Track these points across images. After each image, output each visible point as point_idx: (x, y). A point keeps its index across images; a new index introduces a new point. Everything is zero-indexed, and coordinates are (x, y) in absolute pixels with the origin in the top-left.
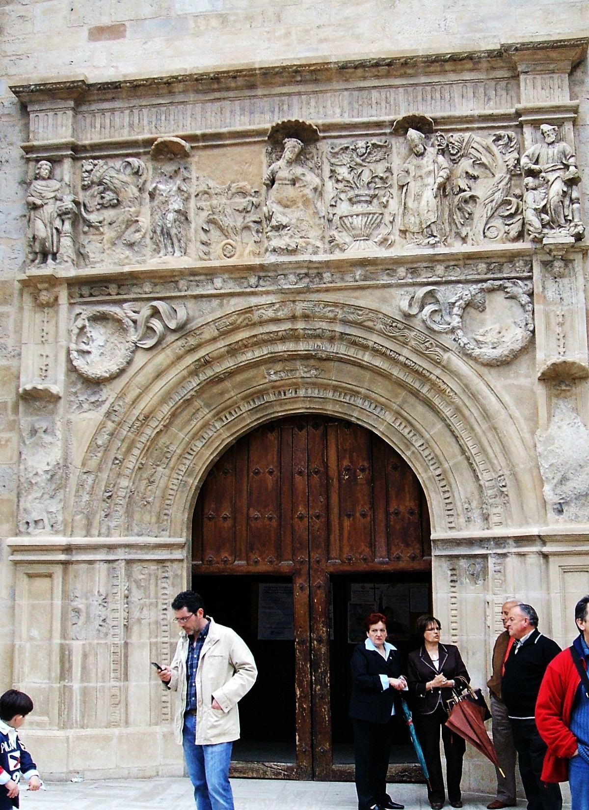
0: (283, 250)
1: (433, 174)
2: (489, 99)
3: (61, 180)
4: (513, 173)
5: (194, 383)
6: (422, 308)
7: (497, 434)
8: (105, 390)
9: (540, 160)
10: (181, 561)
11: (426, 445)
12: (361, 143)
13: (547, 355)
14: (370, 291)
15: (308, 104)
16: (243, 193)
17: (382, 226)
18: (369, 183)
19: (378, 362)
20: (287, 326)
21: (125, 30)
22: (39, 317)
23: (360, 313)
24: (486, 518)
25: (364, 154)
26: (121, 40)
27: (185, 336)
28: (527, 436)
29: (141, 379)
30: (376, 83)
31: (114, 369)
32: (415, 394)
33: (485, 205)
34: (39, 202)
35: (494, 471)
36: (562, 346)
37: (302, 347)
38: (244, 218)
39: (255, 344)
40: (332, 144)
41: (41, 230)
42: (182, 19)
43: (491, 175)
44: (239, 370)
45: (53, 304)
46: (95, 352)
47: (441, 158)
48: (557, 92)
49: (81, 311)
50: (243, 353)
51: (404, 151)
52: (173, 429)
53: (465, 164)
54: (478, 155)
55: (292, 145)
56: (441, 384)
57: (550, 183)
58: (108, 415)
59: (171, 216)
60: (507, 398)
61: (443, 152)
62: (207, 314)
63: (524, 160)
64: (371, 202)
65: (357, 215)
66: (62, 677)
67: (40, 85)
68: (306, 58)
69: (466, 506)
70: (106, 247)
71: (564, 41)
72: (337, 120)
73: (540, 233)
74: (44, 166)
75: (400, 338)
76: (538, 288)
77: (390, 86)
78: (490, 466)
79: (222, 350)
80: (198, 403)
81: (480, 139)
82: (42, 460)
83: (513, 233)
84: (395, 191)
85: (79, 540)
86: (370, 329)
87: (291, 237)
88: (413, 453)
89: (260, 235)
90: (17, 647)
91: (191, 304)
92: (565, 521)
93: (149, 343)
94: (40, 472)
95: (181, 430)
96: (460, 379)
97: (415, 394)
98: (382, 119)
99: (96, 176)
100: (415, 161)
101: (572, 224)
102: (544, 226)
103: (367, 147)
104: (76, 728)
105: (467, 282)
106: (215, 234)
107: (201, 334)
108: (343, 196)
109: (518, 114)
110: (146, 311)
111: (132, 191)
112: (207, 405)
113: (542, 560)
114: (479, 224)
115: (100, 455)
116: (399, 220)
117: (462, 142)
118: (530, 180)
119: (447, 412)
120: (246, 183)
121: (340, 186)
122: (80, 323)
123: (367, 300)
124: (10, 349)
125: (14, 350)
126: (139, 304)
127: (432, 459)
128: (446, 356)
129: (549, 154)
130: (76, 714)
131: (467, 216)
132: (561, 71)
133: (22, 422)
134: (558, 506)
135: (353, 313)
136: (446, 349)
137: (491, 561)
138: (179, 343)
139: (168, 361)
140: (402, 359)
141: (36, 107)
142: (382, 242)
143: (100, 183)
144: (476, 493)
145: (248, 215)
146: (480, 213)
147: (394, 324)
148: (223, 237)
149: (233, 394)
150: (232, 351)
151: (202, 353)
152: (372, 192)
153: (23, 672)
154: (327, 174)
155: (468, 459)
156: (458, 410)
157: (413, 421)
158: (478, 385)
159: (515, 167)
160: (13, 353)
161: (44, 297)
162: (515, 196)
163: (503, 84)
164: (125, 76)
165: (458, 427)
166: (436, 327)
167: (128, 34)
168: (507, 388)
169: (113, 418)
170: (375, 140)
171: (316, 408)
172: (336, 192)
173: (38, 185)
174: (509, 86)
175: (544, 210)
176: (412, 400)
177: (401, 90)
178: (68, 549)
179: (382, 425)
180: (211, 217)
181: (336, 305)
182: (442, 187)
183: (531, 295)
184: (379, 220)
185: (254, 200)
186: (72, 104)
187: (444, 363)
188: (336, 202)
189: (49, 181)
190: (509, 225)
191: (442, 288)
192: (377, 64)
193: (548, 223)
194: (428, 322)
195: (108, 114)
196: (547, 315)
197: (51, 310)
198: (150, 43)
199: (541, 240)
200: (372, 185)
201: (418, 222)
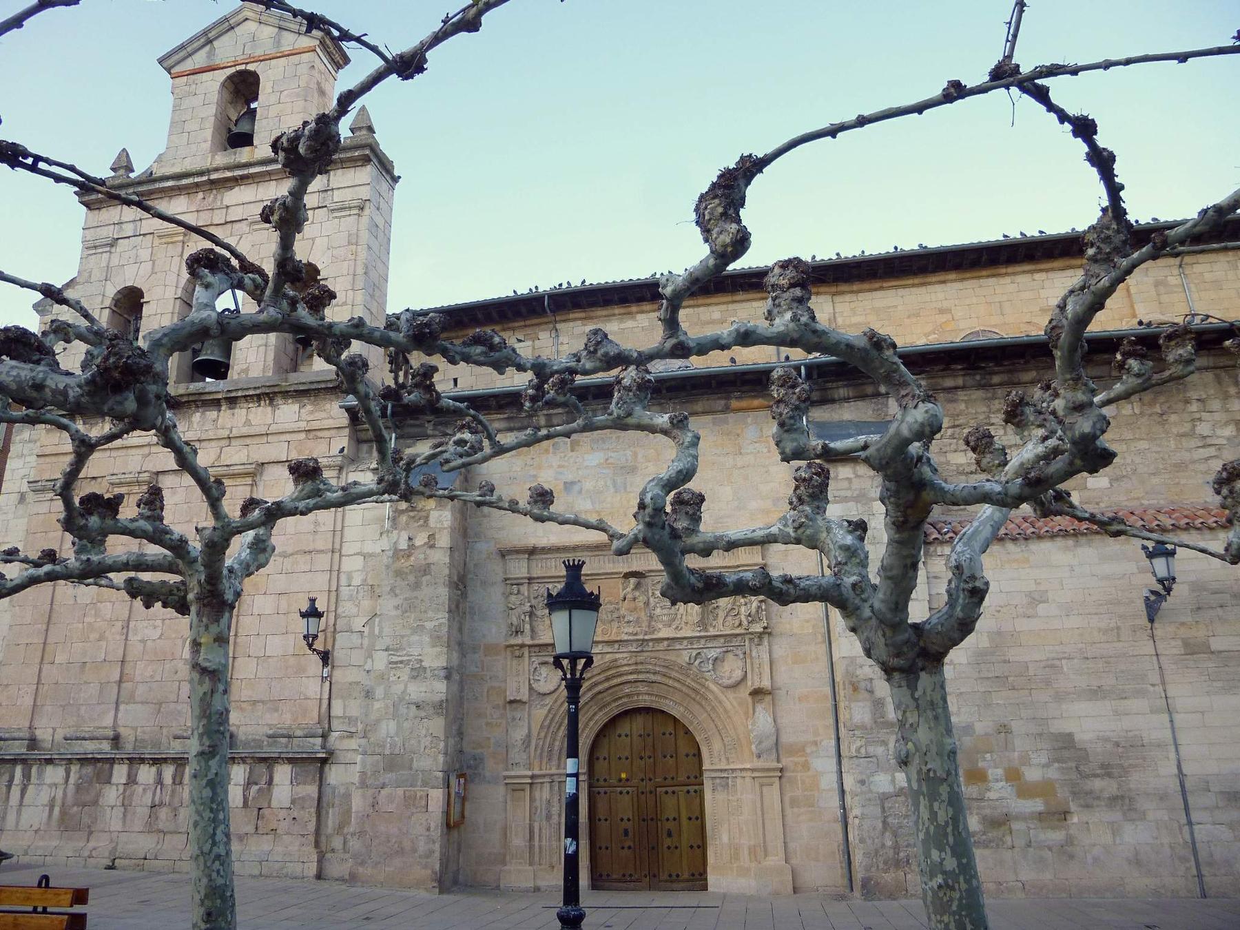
13: (751, 684)
19: (676, 685)
20: (633, 667)
22: (515, 662)
31: (552, 689)
37: (641, 677)
41: (515, 621)
46: (543, 680)
55: (633, 581)
58: (549, 711)
60: (735, 704)
82: (519, 734)
85: (537, 772)
130: (537, 859)
146: (721, 614)
150: (607, 679)
158: (722, 697)
161: (517, 653)
165: (713, 716)
168: (735, 698)
171: (648, 704)
173: (513, 598)
175: (750, 615)
178: (532, 777)
179: (676, 711)
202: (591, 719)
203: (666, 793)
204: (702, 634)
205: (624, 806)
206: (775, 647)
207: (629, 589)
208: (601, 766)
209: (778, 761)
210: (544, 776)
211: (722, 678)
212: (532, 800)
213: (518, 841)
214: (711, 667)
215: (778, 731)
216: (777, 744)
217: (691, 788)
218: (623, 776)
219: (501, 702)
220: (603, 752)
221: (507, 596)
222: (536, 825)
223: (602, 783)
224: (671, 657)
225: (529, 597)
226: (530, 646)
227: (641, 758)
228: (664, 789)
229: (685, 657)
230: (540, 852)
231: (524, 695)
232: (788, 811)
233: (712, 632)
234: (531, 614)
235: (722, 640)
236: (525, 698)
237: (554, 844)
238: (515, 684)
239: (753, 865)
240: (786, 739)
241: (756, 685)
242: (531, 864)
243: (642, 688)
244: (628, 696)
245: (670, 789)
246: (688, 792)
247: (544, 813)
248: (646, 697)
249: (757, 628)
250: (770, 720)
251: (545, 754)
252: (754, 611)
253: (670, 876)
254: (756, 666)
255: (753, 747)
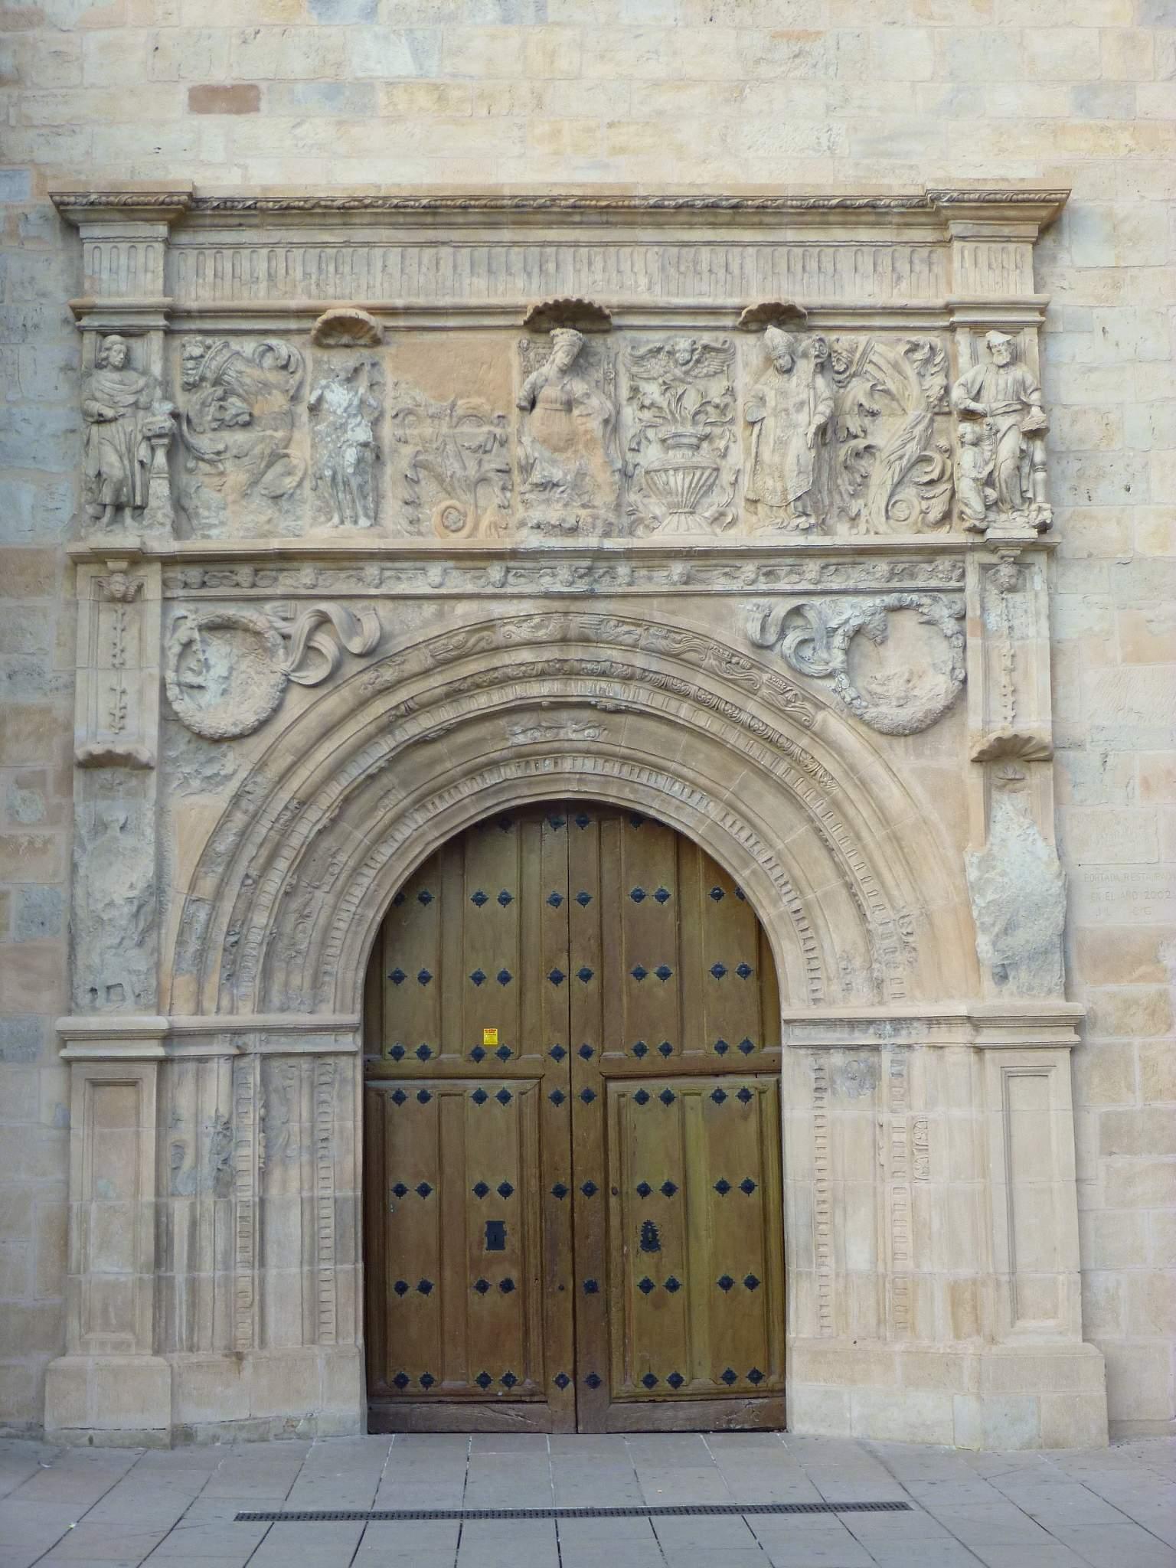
0: (554, 527)
1: (806, 409)
2: (899, 278)
3: (145, 372)
4: (936, 410)
5: (385, 746)
6: (782, 635)
7: (901, 848)
8: (231, 755)
10: (353, 1054)
11: (778, 859)
12: (683, 343)
14: (696, 600)
16: (475, 417)
17: (716, 490)
18: (697, 413)
19: (703, 720)
20: (553, 653)
21: (258, 98)
22: (107, 619)
23: (678, 637)
24: (878, 985)
25: (688, 362)
26: (252, 114)
27: (379, 664)
28: (951, 853)
29: (297, 738)
30: (709, 235)
31: (250, 720)
32: (765, 775)
33: (890, 464)
34: (109, 413)
35: (893, 908)
36: (1010, 707)
37: (579, 689)
38: (480, 462)
39: (492, 683)
40: (633, 340)
41: (114, 465)
42: (365, 86)
43: (900, 412)
44: (463, 724)
45: (130, 599)
46: (213, 688)
47: (820, 382)
49: (185, 613)
50: (472, 696)
51: (756, 359)
52: (345, 826)
53: (857, 391)
54: (879, 375)
55: (565, 338)
56: (808, 761)
57: (999, 435)
58: (236, 799)
59: (351, 455)
60: (919, 791)
61: (822, 367)
62: (416, 626)
63: (957, 394)
64: (698, 447)
66: (158, 1262)
67: (108, 194)
68: (593, 185)
69: (843, 965)
70: (230, 498)
71: (1030, 192)
72: (644, 298)
74: (117, 347)
75: (744, 683)
76: (974, 609)
78: (885, 901)
79: (438, 691)
80: (387, 780)
82: (119, 882)
83: (935, 514)
84: (739, 429)
85: (184, 1019)
86: (694, 666)
88: (754, 872)
89: (508, 494)
90: (75, 1210)
91: (384, 609)
92: (1012, 994)
93: (314, 675)
94: (119, 901)
95: (357, 827)
96: (842, 756)
97: (765, 775)
98: (720, 301)
99: (212, 366)
100: (775, 380)
101: (1034, 506)
102: (988, 508)
103: (693, 351)
104: (181, 1350)
105: (857, 592)
106: (428, 488)
107: (403, 663)
108: (651, 433)
109: (949, 309)
110: (304, 621)
111: (278, 401)
112: (404, 784)
113: (973, 1057)
115: (220, 870)
116: (745, 481)
117: (852, 351)
119: (818, 808)
120: (483, 400)
121: (647, 415)
122: (183, 635)
123: (692, 618)
124: (49, 676)
125: (57, 678)
126: (293, 603)
127: (786, 883)
128: (820, 716)
129: (997, 388)
131: (859, 480)
132: (1020, 239)
133: (80, 810)
134: (999, 970)
135: (666, 638)
136: (820, 706)
137: (886, 1057)
138: (366, 677)
139: (344, 709)
140: (744, 717)
141: (97, 231)
142: (716, 519)
143: (217, 382)
144: (860, 943)
145: (486, 457)
146: (881, 475)
147: (734, 660)
148: (443, 495)
149: (448, 765)
150: (454, 694)
151: (402, 695)
152: (702, 430)
153: (86, 1256)
154: (624, 393)
155: (849, 886)
156: (836, 804)
157: (757, 821)
158: (870, 765)
159: (941, 399)
160: (53, 684)
161: (118, 585)
162: (939, 449)
164: (265, 188)
165: (835, 833)
166: (807, 669)
167: (263, 105)
169: (244, 804)
170: (706, 338)
171: (591, 791)
172: (639, 426)
173: (107, 380)
175: (989, 481)
176: (758, 784)
178: (169, 1037)
179: (690, 815)
180: (421, 457)
181: (637, 622)
182: (822, 430)
183: (961, 618)
185: (498, 431)
186: (162, 230)
187: (816, 728)
188: (639, 444)
189: (124, 373)
191: (816, 601)
193: (996, 503)
194: (794, 661)
195: (228, 253)
196: (986, 654)
197: (129, 608)
198: (306, 126)
200: (702, 418)
201: (779, 489)
202: (382, 837)
203: (642, 1098)
204: (816, 540)
205: (491, 1144)
206: (1069, 601)
207: (549, 370)
208: (410, 1005)
209: (1068, 993)
210: (208, 1034)
211: (876, 698)
212: (165, 1120)
213: (112, 1265)
214: (838, 659)
215: (1069, 890)
216: (1064, 935)
217: (730, 1085)
218: (490, 1038)
219: (46, 760)
220: (415, 955)
221: (79, 374)
222: (180, 1212)
223: (411, 1061)
224: (692, 618)
225: (166, 384)
226: (169, 561)
227: (557, 978)
228: (634, 1087)
229: (745, 620)
230: (193, 1305)
231: (142, 736)
232: (1097, 1167)
233: (844, 535)
234: (176, 444)
235: (882, 567)
236: (147, 751)
237: (244, 1274)
238: (105, 704)
239: (970, 1347)
240: (1092, 919)
241: (1001, 728)
242: (159, 1349)
243: (574, 731)
244: (523, 756)
245: (655, 1088)
246: (719, 1097)
247: (207, 1170)
248: (588, 765)
249: (1016, 526)
250: (1045, 850)
251: (216, 957)
252: (1006, 468)
253: (650, 1381)
254: (999, 664)
255: (983, 943)
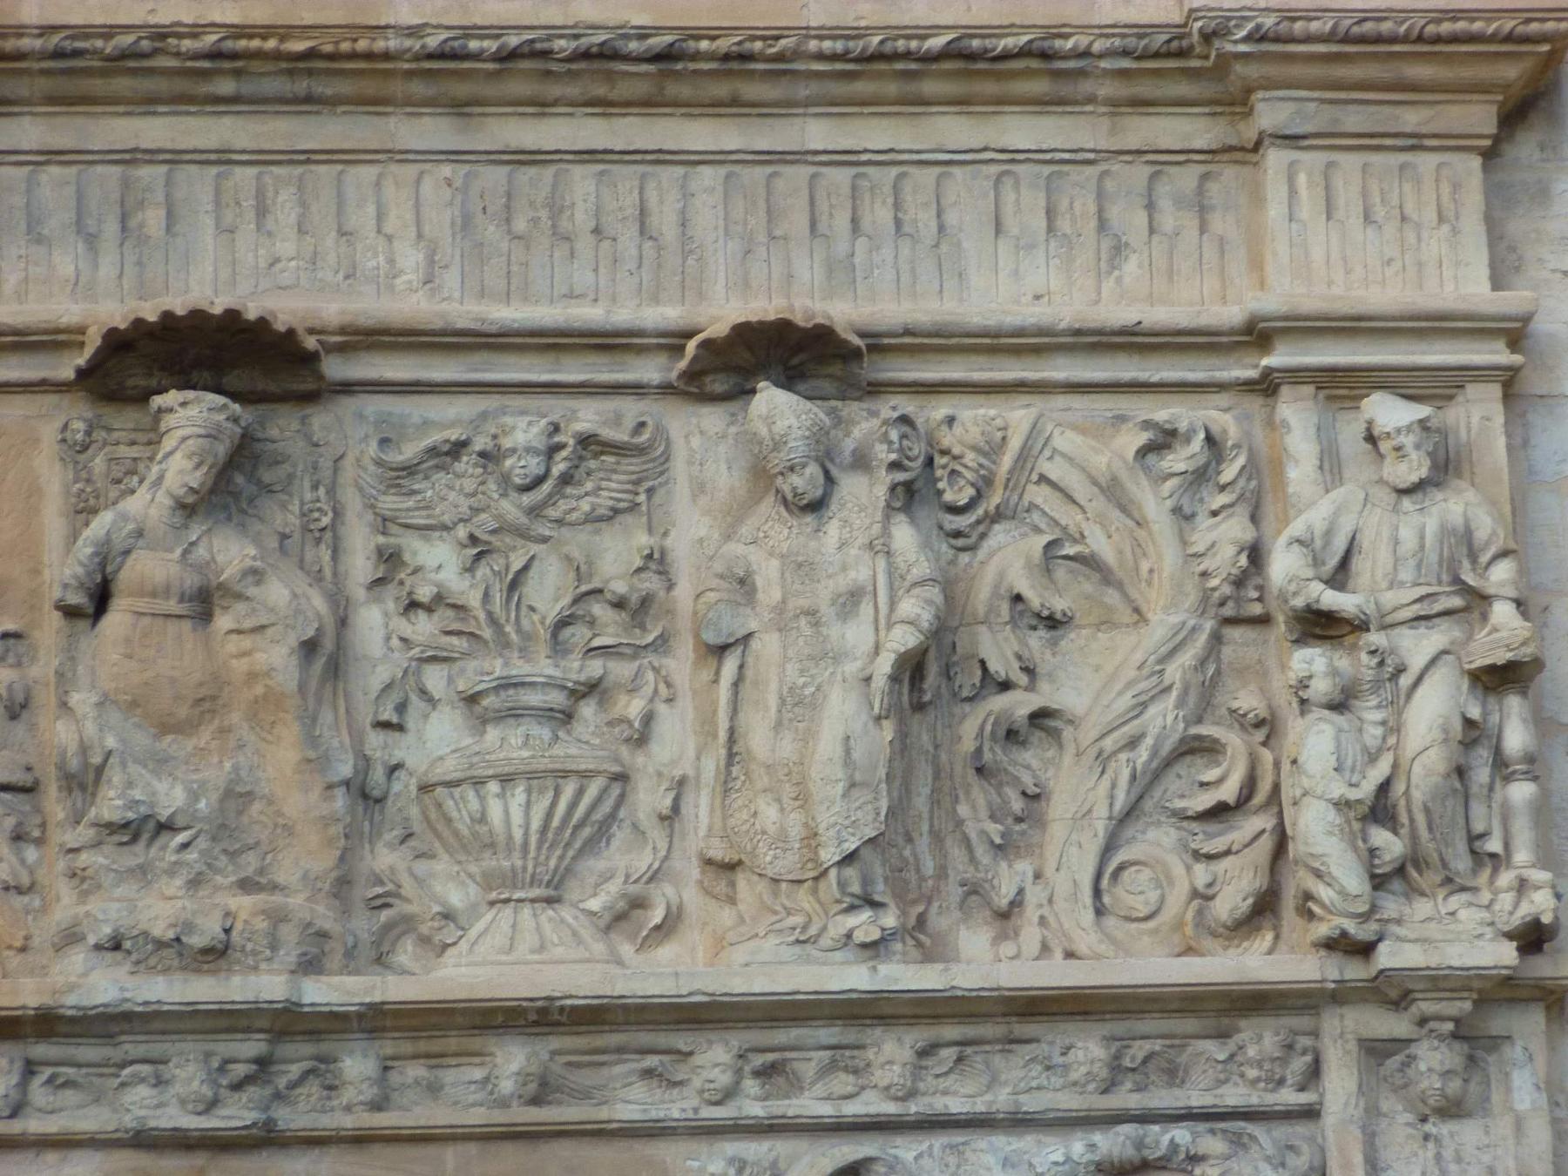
0: (160, 944)
1: (866, 609)
2: (1119, 249)
4: (1229, 611)
9: (1358, 564)
12: (523, 430)
15: (262, 211)
17: (620, 835)
18: (563, 623)
25: (539, 481)
33: (1104, 760)
40: (382, 420)
43: (1127, 617)
47: (904, 535)
48: (1434, 244)
51: (726, 477)
53: (1008, 558)
54: (1068, 517)
55: (191, 419)
57: (1405, 681)
63: (1284, 565)
64: (568, 717)
65: (506, 780)
72: (409, 305)
73: (1365, 917)
77: (661, 157)
81: (1081, 445)
83: (1232, 900)
84: (681, 664)
87: (195, 883)
89: (31, 854)
98: (624, 315)
100: (785, 532)
102: (1378, 882)
105: (1019, 1122)
108: (435, 678)
114: (1069, 849)
116: (701, 808)
118: (1314, 663)
121: (423, 627)
129: (1397, 549)
131: (1017, 805)
142: (620, 917)
146: (1079, 794)
152: (577, 669)
154: (360, 566)
159: (1239, 582)
162: (1239, 719)
163: (1186, 178)
170: (588, 416)
172: (401, 658)
174: (1213, 188)
175: (1380, 809)
177: (708, 176)
182: (912, 668)
184: (606, 807)
188: (401, 708)
190: (1210, 857)
192: (601, 56)
193: (1400, 871)
199: (1365, 950)
200: (578, 634)
207: (146, 504)
233: (979, 962)
235: (1088, 1049)
